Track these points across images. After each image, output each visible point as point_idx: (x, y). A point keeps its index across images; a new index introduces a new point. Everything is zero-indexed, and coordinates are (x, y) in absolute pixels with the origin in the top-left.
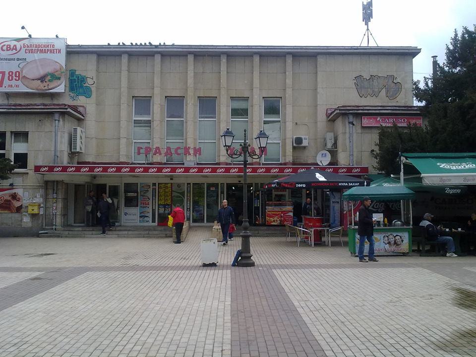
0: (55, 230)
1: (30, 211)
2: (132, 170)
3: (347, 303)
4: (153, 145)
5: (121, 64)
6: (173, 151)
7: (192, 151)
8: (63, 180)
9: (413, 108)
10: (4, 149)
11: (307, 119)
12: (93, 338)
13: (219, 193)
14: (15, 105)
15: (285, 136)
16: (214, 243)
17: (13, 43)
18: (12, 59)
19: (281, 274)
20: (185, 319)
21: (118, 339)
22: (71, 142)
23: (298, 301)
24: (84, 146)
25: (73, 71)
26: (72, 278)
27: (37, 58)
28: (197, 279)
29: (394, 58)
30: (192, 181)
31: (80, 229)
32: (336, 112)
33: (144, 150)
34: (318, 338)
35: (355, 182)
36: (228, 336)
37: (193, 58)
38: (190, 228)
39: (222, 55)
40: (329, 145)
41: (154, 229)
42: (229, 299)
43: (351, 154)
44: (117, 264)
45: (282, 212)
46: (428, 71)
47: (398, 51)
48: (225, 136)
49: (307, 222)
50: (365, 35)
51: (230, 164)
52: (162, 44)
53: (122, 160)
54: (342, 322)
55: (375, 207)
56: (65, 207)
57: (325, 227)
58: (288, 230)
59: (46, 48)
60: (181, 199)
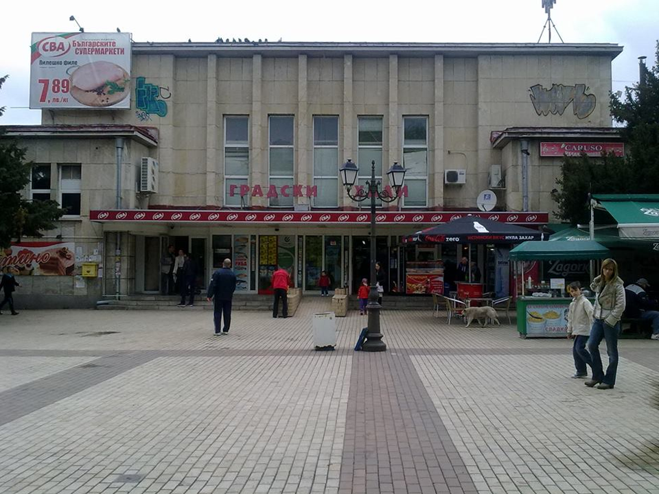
0: (119, 299)
1: (84, 273)
2: (223, 217)
3: (506, 402)
4: (251, 184)
5: (206, 70)
6: (278, 191)
7: (304, 191)
8: (128, 231)
9: (611, 131)
10: (48, 187)
11: (464, 145)
12: (159, 446)
13: (343, 249)
14: (63, 127)
15: (434, 170)
16: (331, 318)
17: (58, 41)
18: (58, 62)
19: (421, 362)
20: (284, 421)
21: (191, 449)
22: (140, 178)
23: (440, 399)
24: (157, 184)
25: (141, 79)
26: (138, 365)
27: (91, 62)
28: (306, 367)
29: (585, 60)
30: (305, 232)
31: (153, 298)
32: (504, 136)
33: (239, 189)
34: (461, 448)
35: (528, 235)
36: (339, 445)
37: (306, 60)
38: (302, 298)
39: (300, 56)
40: (495, 183)
41: (253, 299)
42: (346, 395)
43: (525, 194)
44: (199, 347)
45: (429, 276)
46: (634, 79)
47: (590, 50)
48: (345, 170)
49: (462, 290)
50: (545, 27)
51: (357, 209)
52: (263, 41)
53: (209, 203)
54: (496, 429)
55: (572, 269)
56: (133, 268)
57: (487, 297)
58: (436, 301)
59: (103, 46)
60: (289, 257)
